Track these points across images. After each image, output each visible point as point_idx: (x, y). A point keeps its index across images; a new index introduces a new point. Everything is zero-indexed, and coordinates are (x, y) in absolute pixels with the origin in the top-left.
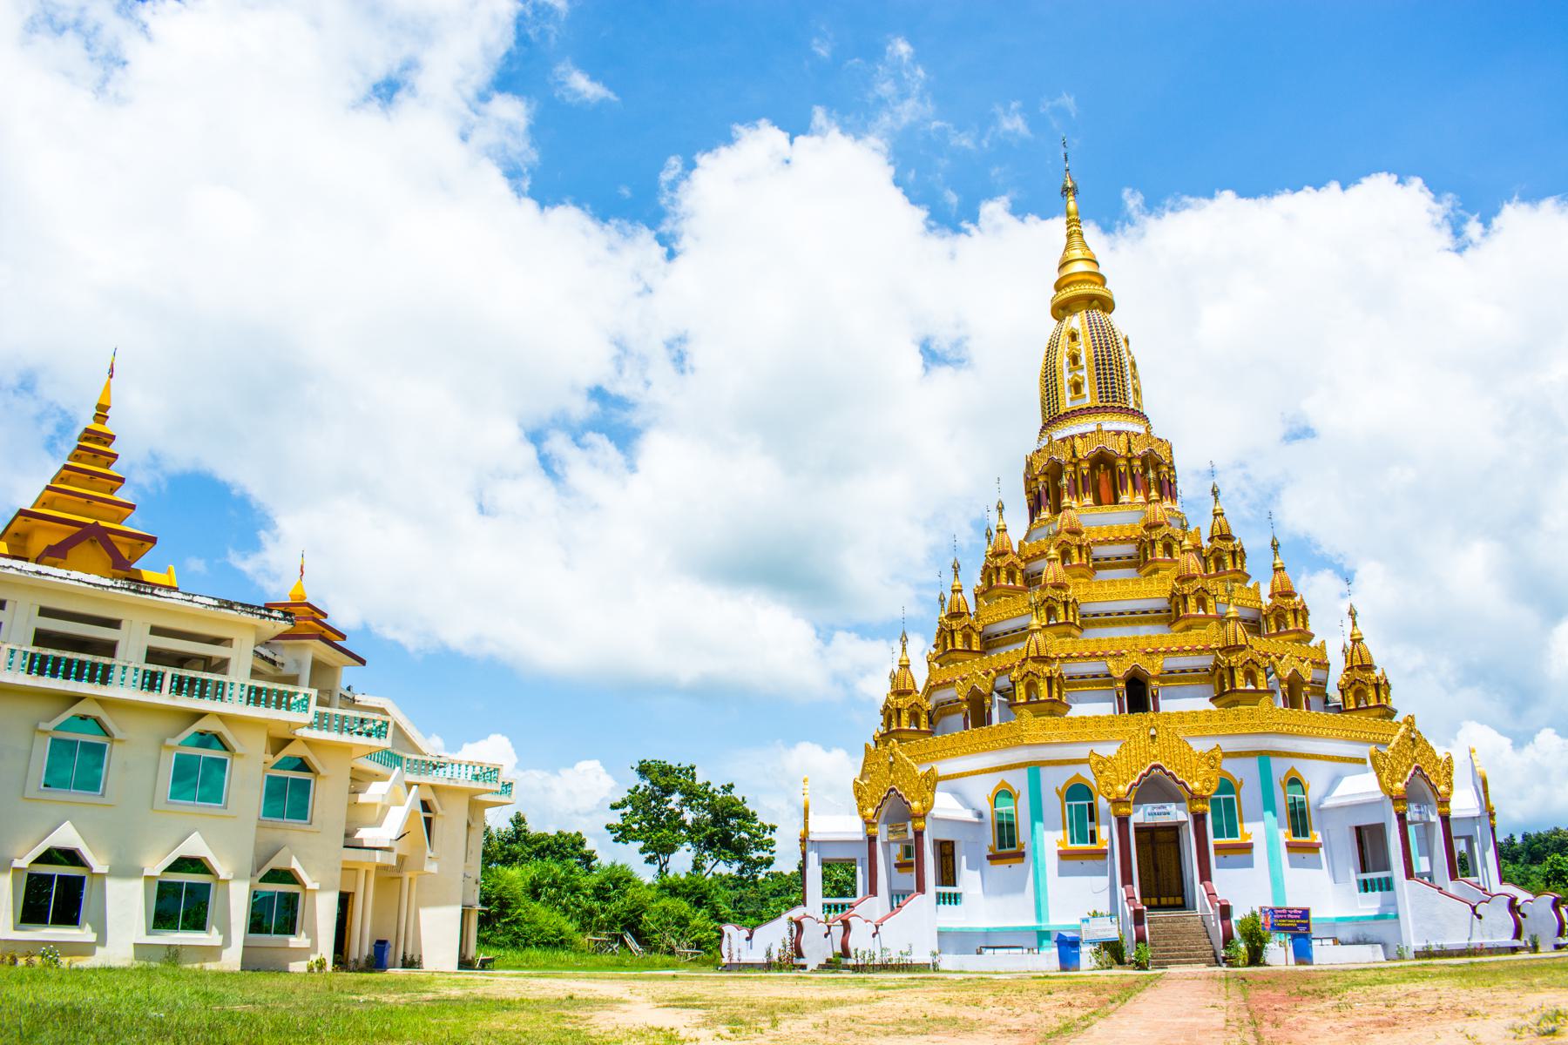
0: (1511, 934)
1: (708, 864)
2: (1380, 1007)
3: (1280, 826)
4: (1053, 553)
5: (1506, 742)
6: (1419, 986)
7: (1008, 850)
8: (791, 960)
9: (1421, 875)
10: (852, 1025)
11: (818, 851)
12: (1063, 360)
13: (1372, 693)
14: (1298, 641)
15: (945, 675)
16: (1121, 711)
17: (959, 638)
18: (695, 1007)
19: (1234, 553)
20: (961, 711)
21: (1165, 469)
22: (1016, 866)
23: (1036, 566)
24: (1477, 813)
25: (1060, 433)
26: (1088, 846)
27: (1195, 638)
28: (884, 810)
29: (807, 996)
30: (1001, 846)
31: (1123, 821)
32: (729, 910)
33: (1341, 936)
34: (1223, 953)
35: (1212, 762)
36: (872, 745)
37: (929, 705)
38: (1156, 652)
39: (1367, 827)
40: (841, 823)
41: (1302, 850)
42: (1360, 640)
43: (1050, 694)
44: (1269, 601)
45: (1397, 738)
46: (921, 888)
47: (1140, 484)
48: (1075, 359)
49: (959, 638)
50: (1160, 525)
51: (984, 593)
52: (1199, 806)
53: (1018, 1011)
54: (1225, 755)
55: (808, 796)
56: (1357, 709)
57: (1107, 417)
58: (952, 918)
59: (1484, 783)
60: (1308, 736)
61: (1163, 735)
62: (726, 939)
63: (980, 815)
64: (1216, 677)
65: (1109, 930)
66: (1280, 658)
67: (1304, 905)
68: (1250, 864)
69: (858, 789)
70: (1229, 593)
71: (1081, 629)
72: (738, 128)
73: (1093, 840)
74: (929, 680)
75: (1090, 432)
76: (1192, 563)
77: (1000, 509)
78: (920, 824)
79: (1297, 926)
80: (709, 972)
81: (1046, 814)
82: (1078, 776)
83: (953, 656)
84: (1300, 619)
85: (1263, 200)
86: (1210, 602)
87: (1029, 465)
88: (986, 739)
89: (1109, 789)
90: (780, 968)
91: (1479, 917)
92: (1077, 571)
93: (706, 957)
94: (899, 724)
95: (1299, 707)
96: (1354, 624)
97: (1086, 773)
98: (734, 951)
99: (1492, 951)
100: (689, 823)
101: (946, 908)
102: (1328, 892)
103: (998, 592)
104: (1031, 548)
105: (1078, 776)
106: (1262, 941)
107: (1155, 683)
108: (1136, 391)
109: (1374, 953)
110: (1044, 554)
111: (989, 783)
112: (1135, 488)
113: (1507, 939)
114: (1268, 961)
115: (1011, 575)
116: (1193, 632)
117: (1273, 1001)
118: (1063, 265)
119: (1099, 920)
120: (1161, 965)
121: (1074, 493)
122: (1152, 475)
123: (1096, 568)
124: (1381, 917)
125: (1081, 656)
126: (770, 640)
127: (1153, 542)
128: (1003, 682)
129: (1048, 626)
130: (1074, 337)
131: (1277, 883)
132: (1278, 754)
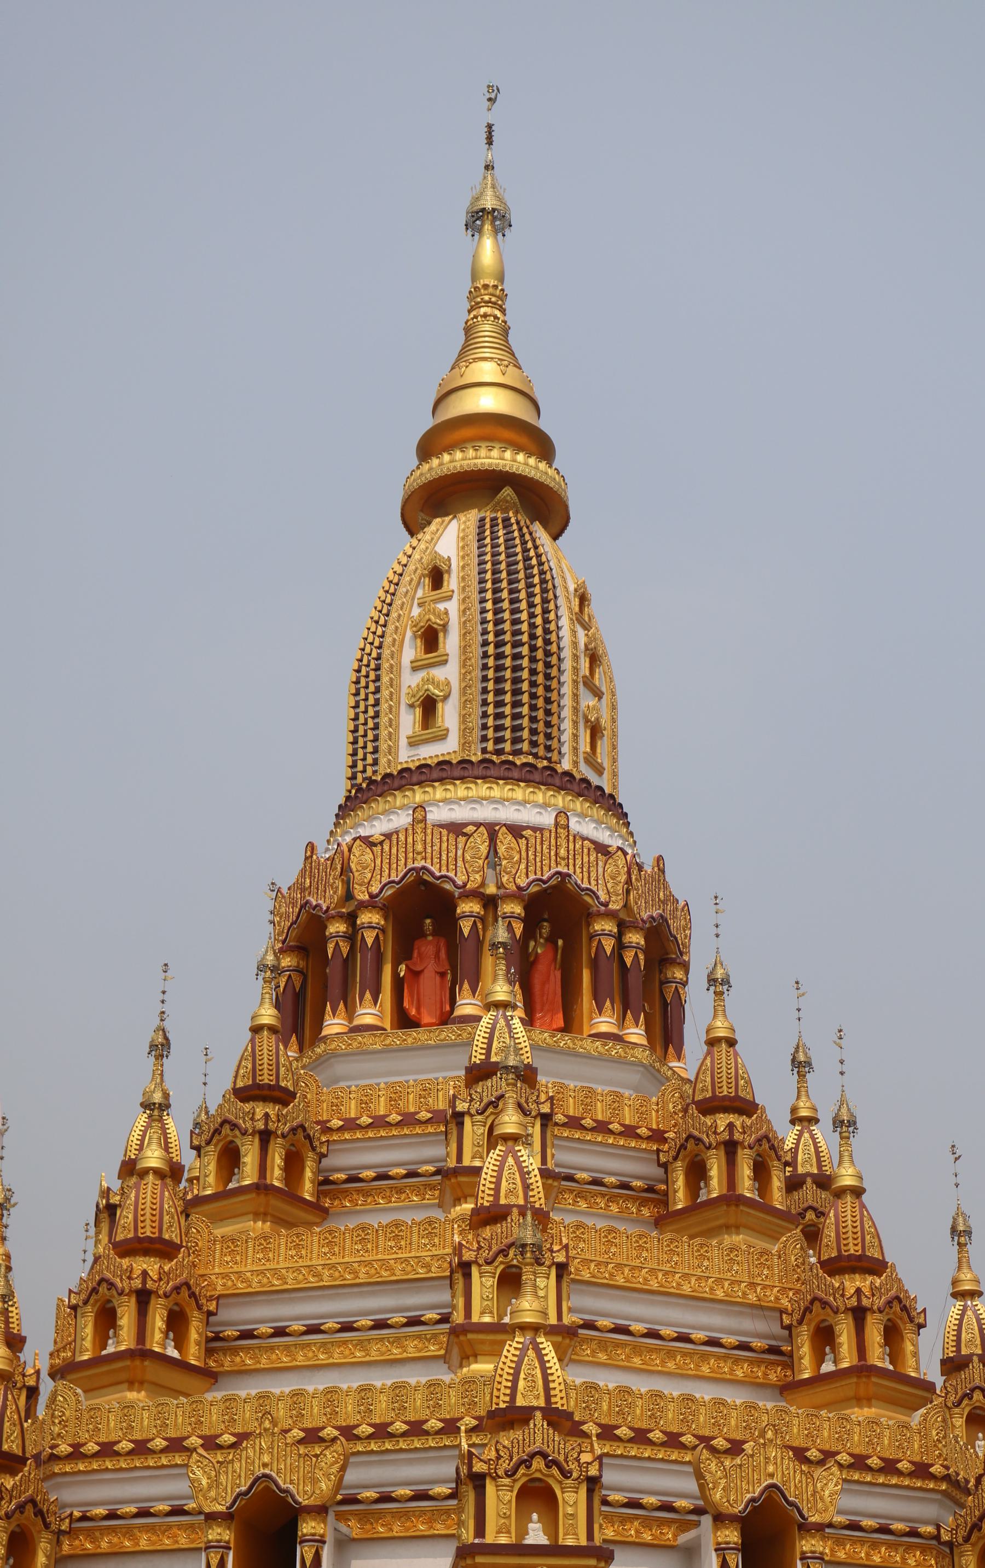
25: (386, 818)
57: (439, 792)
75: (489, 826)
130: (437, 577)
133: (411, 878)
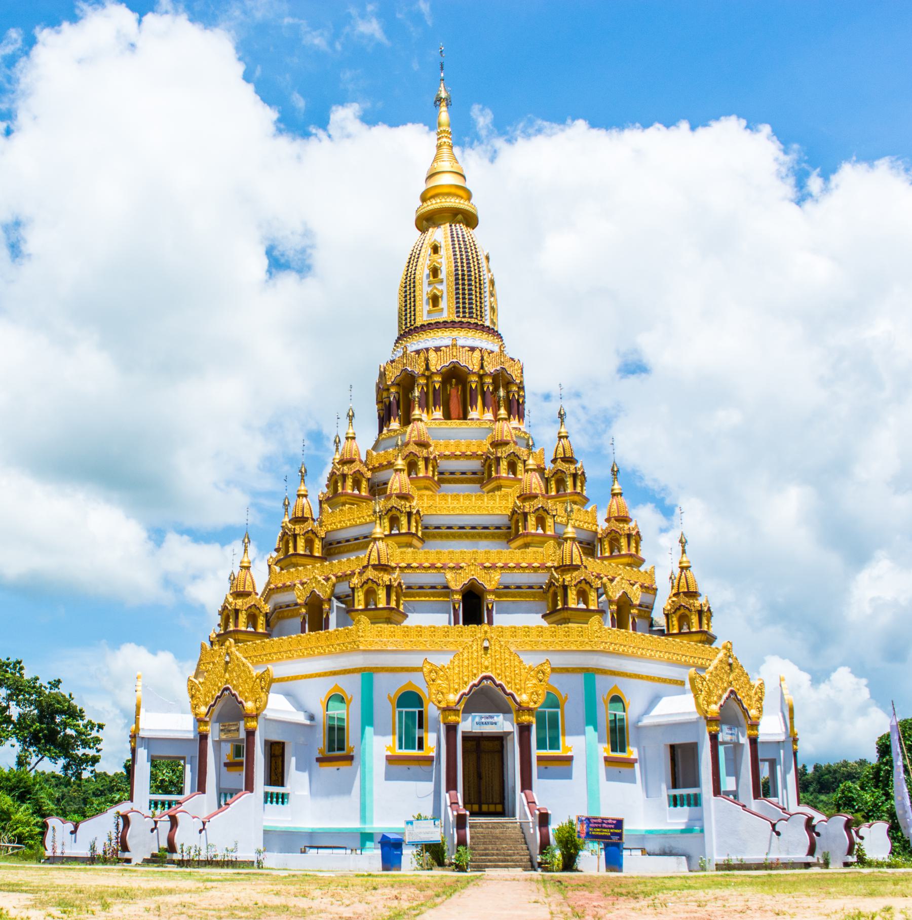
0: (806, 850)
1: (34, 759)
2: (693, 906)
3: (600, 740)
4: (400, 463)
5: (805, 678)
6: (725, 892)
7: (337, 753)
8: (118, 853)
9: (727, 793)
10: (184, 910)
11: (148, 747)
12: (423, 271)
13: (695, 619)
14: (629, 565)
15: (286, 578)
16: (456, 622)
17: (301, 543)
18: (22, 891)
19: (575, 476)
20: (299, 614)
21: (515, 388)
22: (344, 768)
23: (382, 476)
24: (782, 738)
26: (415, 752)
27: (532, 556)
28: (217, 709)
29: (135, 885)
30: (331, 748)
31: (451, 729)
32: (52, 806)
33: (649, 847)
34: (539, 859)
35: (541, 676)
36: (208, 645)
37: (267, 608)
38: (493, 567)
39: (681, 746)
40: (173, 722)
41: (618, 766)
42: (687, 568)
43: (388, 602)
44: (605, 525)
45: (715, 662)
46: (249, 787)
47: (491, 402)
48: (435, 272)
49: (301, 543)
50: (506, 443)
51: (328, 499)
52: (526, 718)
53: (347, 902)
54: (553, 670)
55: (138, 696)
56: (680, 634)
58: (279, 818)
59: (791, 710)
60: (633, 656)
61: (495, 647)
62: (50, 834)
63: (312, 718)
64: (550, 594)
65: (433, 833)
66: (612, 580)
67: (619, 817)
68: (568, 776)
69: (192, 687)
70: (569, 513)
71: (422, 540)
72: (84, 6)
73: (421, 747)
74: (269, 583)
75: (446, 347)
76: (535, 482)
77: (351, 417)
78: (252, 724)
79: (611, 836)
80: (34, 865)
81: (376, 721)
82: (410, 684)
83: (294, 560)
84: (633, 544)
85: (614, 132)
86: (549, 522)
87: (382, 375)
88: (323, 643)
89: (440, 697)
90: (105, 861)
91: (778, 834)
92: (422, 483)
93: (28, 851)
94: (236, 625)
95: (626, 628)
96: (684, 552)
97: (419, 683)
98: (58, 845)
99: (786, 865)
100: (15, 718)
101: (272, 807)
102: (641, 806)
103: (343, 499)
104: (378, 458)
105: (410, 684)
106: (577, 848)
107: (491, 597)
108: (493, 309)
109: (679, 864)
110: (390, 464)
111: (324, 687)
112: (484, 405)
113: (801, 855)
114: (579, 868)
115: (357, 484)
116: (531, 549)
117: (590, 899)
118: (430, 176)
119: (422, 823)
120: (480, 868)
121: (425, 406)
122: (502, 393)
123: (441, 481)
124: (688, 830)
125: (421, 567)
126: (101, 539)
127: (498, 459)
128: (343, 588)
129: (390, 535)
130: (435, 249)
131: (593, 794)
132: (604, 672)
133: (451, 366)
